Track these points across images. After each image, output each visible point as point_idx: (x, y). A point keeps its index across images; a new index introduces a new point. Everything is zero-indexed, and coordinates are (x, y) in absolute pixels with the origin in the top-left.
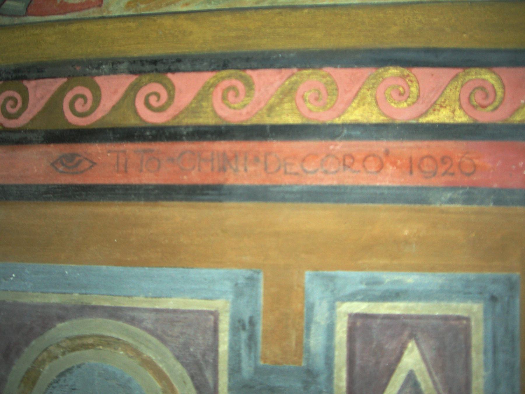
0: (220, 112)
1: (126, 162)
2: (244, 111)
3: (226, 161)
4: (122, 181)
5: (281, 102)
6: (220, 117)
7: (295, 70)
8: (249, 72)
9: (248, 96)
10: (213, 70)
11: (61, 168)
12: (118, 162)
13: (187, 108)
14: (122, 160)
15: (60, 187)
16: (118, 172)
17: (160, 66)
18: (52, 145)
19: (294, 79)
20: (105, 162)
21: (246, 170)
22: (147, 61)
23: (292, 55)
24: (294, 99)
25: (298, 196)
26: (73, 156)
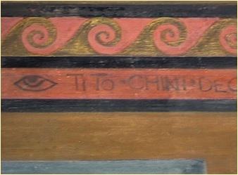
0: (160, 48)
1: (84, 83)
2: (180, 47)
3: (167, 84)
4: (81, 96)
5: (208, 42)
6: (160, 51)
7: (217, 19)
8: (181, 19)
9: (182, 37)
10: (152, 17)
11: (25, 87)
12: (76, 83)
13: (87, 37)
14: (80, 81)
15: (24, 101)
16: (77, 90)
17: (106, 12)
18: (14, 69)
19: (217, 25)
20: (63, 84)
21: (185, 89)
22: (95, 8)
23: (214, 8)
24: (217, 40)
25: (227, 107)
26: (35, 78)
